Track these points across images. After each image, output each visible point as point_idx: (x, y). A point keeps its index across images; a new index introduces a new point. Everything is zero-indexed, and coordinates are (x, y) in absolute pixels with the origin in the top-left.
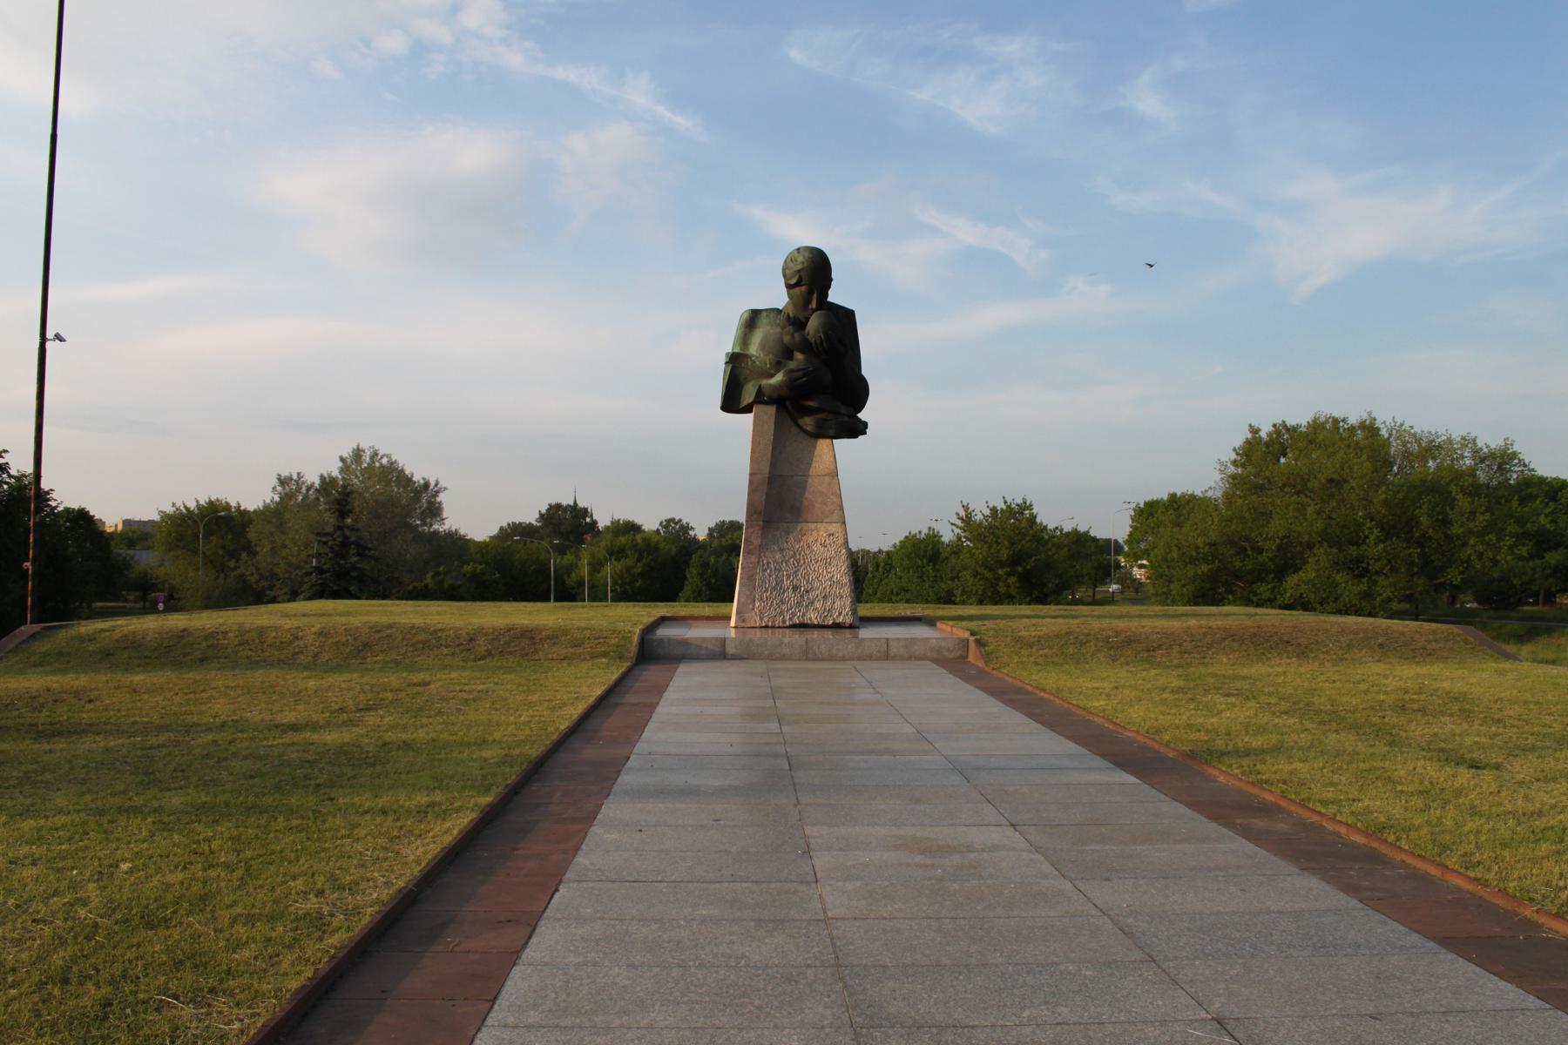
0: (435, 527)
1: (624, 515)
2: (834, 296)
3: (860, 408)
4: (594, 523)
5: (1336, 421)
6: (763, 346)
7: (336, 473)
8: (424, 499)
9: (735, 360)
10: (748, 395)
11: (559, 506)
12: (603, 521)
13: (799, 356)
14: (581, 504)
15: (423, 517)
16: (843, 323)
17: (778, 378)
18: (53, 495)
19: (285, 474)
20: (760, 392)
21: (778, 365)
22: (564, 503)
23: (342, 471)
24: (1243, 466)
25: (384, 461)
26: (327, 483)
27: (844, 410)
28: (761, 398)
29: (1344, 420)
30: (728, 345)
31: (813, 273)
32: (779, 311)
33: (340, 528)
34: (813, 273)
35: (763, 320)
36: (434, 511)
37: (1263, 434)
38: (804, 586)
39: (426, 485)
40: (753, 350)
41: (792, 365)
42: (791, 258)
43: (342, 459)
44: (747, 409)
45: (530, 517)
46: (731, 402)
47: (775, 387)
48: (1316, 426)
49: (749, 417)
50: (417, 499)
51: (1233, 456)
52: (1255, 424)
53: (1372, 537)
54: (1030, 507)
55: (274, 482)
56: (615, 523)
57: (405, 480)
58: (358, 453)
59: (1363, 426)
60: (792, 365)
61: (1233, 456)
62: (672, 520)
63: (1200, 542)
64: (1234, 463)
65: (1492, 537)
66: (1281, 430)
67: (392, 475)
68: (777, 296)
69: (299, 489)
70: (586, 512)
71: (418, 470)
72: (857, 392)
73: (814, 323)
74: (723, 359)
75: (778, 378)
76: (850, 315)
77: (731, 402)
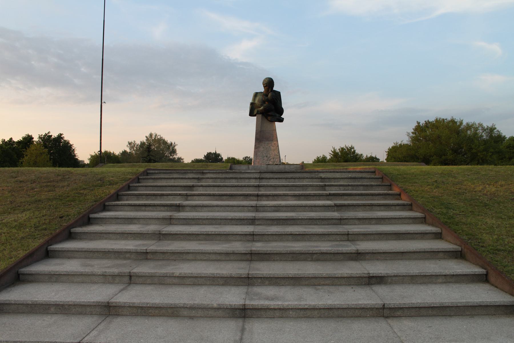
0: (174, 156)
1: (231, 156)
2: (274, 89)
3: (282, 114)
4: (222, 158)
5: (443, 120)
6: (258, 101)
7: (145, 141)
8: (171, 148)
9: (252, 104)
10: (255, 112)
11: (210, 153)
12: (225, 158)
13: (267, 103)
14: (218, 152)
15: (171, 153)
16: (278, 94)
17: (262, 108)
18: (74, 146)
19: (130, 141)
20: (258, 111)
21: (262, 105)
22: (212, 152)
23: (146, 140)
24: (415, 134)
25: (159, 137)
26: (143, 144)
27: (277, 115)
28: (257, 113)
29: (446, 119)
30: (250, 100)
31: (269, 83)
32: (262, 92)
33: (149, 155)
34: (269, 83)
35: (259, 95)
36: (174, 152)
37: (421, 124)
38: (269, 156)
39: (172, 144)
40: (256, 102)
41: (265, 105)
42: (264, 80)
43: (146, 137)
44: (255, 116)
45: (201, 157)
46: (251, 114)
47: (261, 110)
48: (437, 121)
49: (255, 117)
50: (169, 148)
51: (413, 131)
52: (419, 121)
53: (449, 154)
54: (353, 148)
55: (127, 144)
56: (229, 159)
57: (165, 142)
58: (151, 135)
59: (451, 120)
60: (265, 105)
61: (413, 131)
62: (247, 157)
63: (400, 156)
64: (413, 133)
65: (485, 153)
66: (427, 123)
67: (161, 142)
68: (262, 89)
69: (134, 146)
70: (219, 155)
71: (169, 139)
72: (281, 111)
73: (270, 95)
74: (249, 104)
75: (262, 108)
76: (279, 93)
77: (251, 114)
